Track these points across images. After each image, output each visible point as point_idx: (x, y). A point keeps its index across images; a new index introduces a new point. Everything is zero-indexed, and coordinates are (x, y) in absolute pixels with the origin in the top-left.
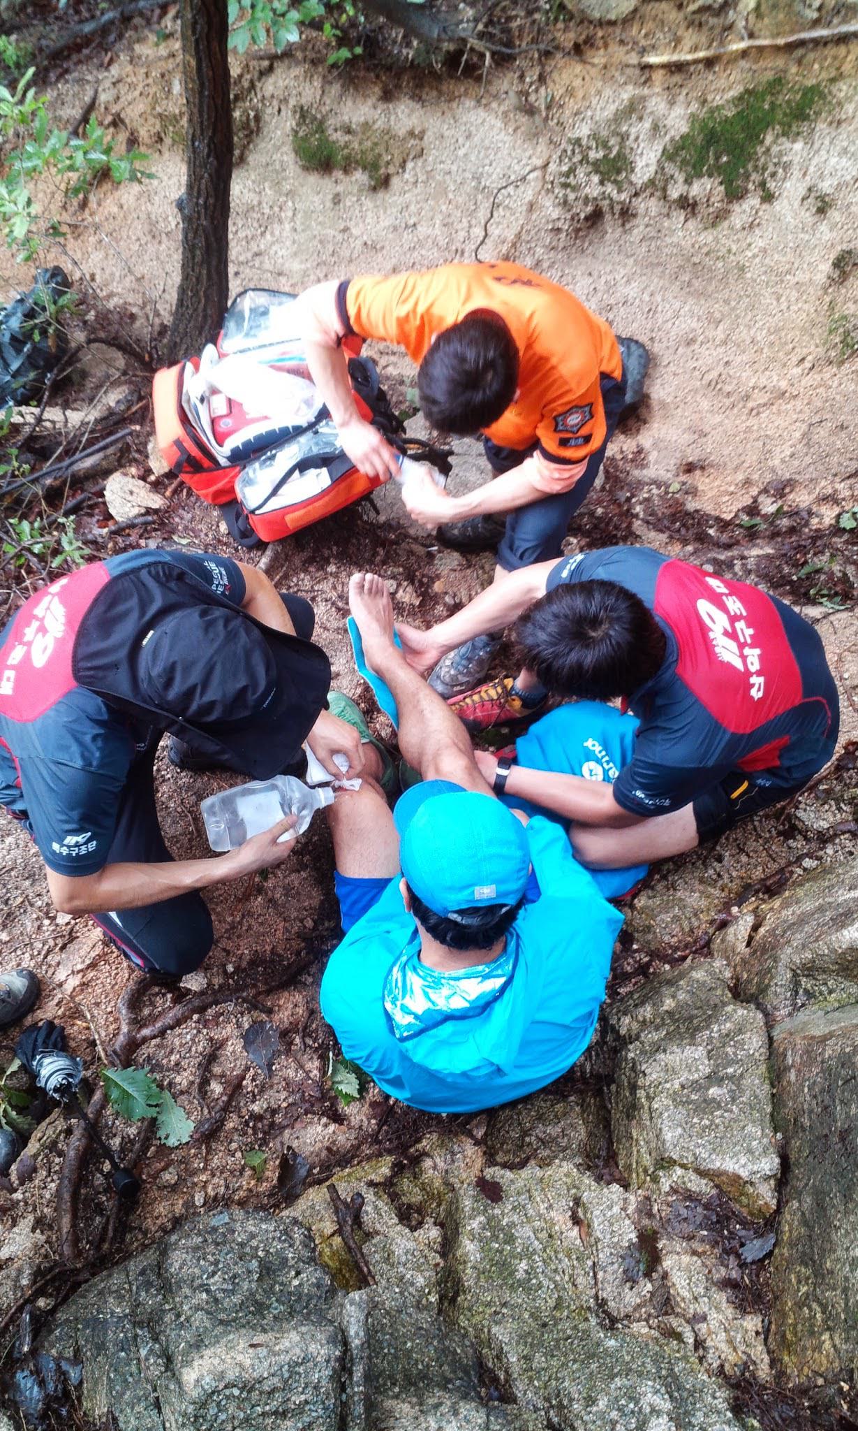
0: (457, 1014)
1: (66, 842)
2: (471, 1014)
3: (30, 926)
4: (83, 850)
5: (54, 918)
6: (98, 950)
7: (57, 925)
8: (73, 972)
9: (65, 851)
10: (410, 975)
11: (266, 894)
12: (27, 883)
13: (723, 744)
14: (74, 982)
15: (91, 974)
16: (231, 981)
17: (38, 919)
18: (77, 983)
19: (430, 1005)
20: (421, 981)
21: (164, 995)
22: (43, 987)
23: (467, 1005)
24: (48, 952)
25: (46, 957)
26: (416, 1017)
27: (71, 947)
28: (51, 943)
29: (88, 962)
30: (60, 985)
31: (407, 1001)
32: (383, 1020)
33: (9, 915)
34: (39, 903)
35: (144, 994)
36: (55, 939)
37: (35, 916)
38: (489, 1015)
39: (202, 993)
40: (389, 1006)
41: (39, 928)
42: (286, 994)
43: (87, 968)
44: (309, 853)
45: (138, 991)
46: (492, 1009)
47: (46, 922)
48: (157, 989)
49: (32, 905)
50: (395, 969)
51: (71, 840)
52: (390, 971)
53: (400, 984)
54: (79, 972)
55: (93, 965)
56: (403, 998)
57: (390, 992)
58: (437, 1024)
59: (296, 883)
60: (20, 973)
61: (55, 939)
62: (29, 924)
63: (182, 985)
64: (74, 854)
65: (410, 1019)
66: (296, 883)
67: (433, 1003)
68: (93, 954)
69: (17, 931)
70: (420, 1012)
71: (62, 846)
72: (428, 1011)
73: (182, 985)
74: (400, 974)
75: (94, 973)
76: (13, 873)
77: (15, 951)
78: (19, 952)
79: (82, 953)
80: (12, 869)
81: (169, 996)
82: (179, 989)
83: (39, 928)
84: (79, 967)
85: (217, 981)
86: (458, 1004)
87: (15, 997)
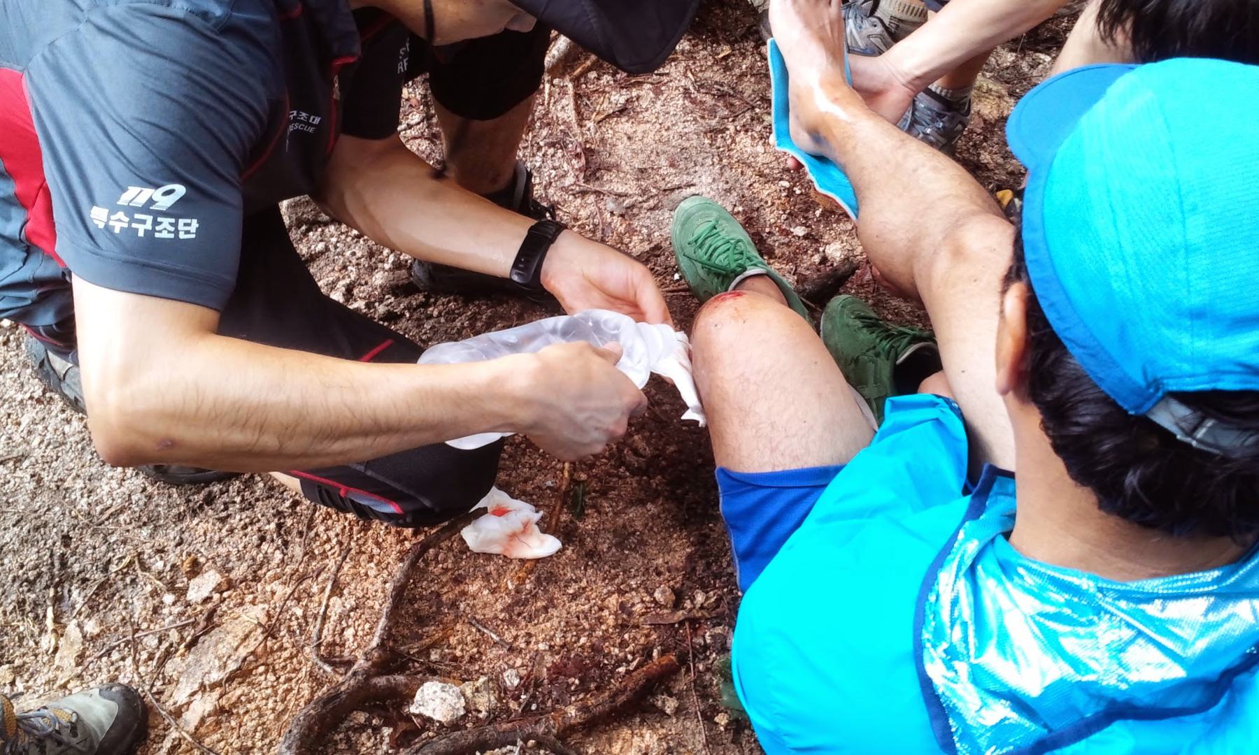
0: (1144, 699)
1: (124, 199)
2: (1175, 704)
3: (139, 608)
4: (165, 230)
5: (183, 592)
6: (252, 644)
7: (188, 605)
8: (203, 687)
9: (119, 222)
10: (989, 585)
11: (582, 542)
12: (145, 532)
13: (1249, 566)
14: (203, 706)
15: (237, 691)
16: (513, 705)
17: (155, 593)
18: (209, 707)
19: (1067, 671)
20: (1031, 605)
21: (376, 730)
22: (151, 721)
23: (1177, 672)
24: (168, 654)
25: (162, 664)
26: (1019, 703)
27: (207, 641)
28: (174, 636)
29: (232, 666)
30: (178, 713)
31: (991, 659)
32: (920, 716)
33: (102, 587)
34: (160, 565)
35: (335, 727)
36: (181, 629)
37: (149, 588)
38: (1229, 709)
39: (456, 725)
40: (936, 671)
41: (156, 610)
42: (626, 733)
43: (230, 679)
44: (662, 471)
45: (321, 718)
46: (1243, 689)
47: (169, 598)
48: (361, 717)
49: (145, 568)
50: (946, 577)
51: (137, 195)
52: (929, 581)
53: (966, 611)
54: (213, 686)
55: (242, 674)
56: (980, 650)
57: (938, 634)
58: (1085, 729)
59: (638, 525)
60: (104, 692)
61: (181, 629)
62: (138, 604)
63: (413, 709)
64: (141, 230)
65: (1000, 711)
66: (638, 525)
67: (1075, 663)
68: (243, 652)
69: (115, 618)
70: (1032, 688)
71: (114, 209)
72: (1058, 689)
73: (413, 709)
74: (963, 586)
75: (244, 688)
76: (122, 518)
77: (109, 653)
78: (115, 656)
79: (223, 649)
80: (121, 511)
81: (387, 731)
82: (408, 718)
83: (156, 610)
84: (216, 676)
85: (485, 702)
86: (1151, 669)
87: (88, 736)
